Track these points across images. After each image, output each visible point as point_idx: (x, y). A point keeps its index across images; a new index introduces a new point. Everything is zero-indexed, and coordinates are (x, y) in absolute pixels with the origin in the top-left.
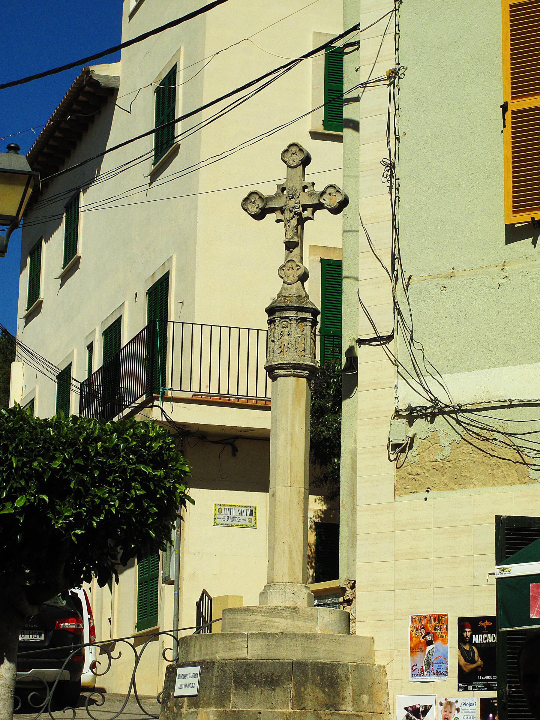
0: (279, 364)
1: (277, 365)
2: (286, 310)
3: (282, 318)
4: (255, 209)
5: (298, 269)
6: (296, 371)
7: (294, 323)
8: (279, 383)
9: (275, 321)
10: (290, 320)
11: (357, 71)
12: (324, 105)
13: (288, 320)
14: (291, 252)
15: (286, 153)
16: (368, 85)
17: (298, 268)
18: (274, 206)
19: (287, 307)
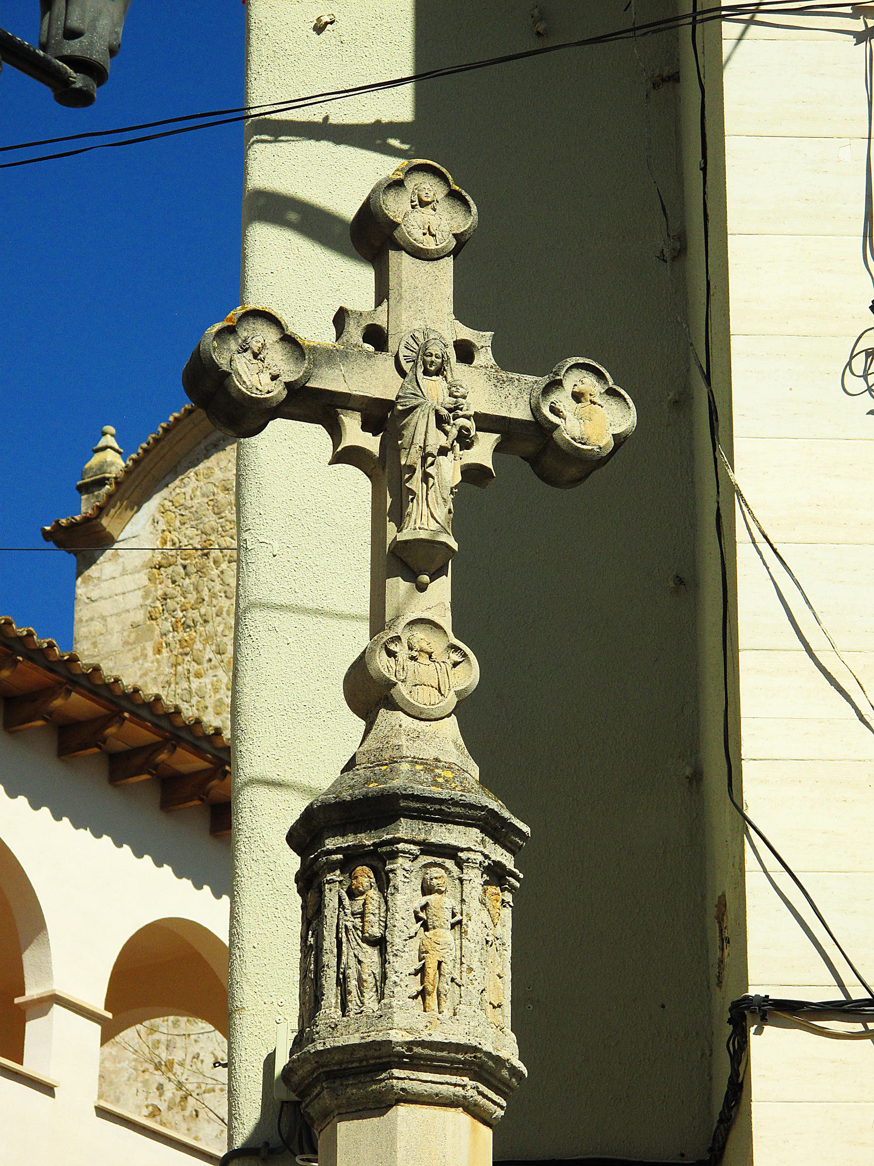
0: (422, 1044)
1: (410, 1044)
2: (446, 819)
3: (428, 849)
4: (265, 378)
5: (455, 664)
6: (482, 1088)
7: (475, 877)
8: (401, 1127)
9: (394, 855)
10: (460, 864)
11: (319, 29)
12: (415, 78)
13: (449, 864)
14: (422, 588)
15: (392, 193)
16: (759, 17)
17: (456, 657)
18: (341, 388)
19: (456, 803)
